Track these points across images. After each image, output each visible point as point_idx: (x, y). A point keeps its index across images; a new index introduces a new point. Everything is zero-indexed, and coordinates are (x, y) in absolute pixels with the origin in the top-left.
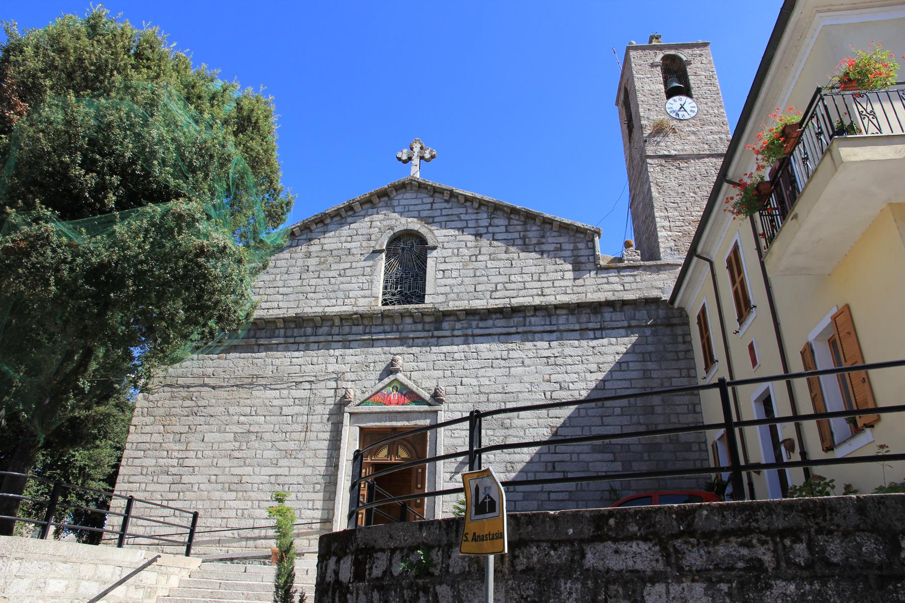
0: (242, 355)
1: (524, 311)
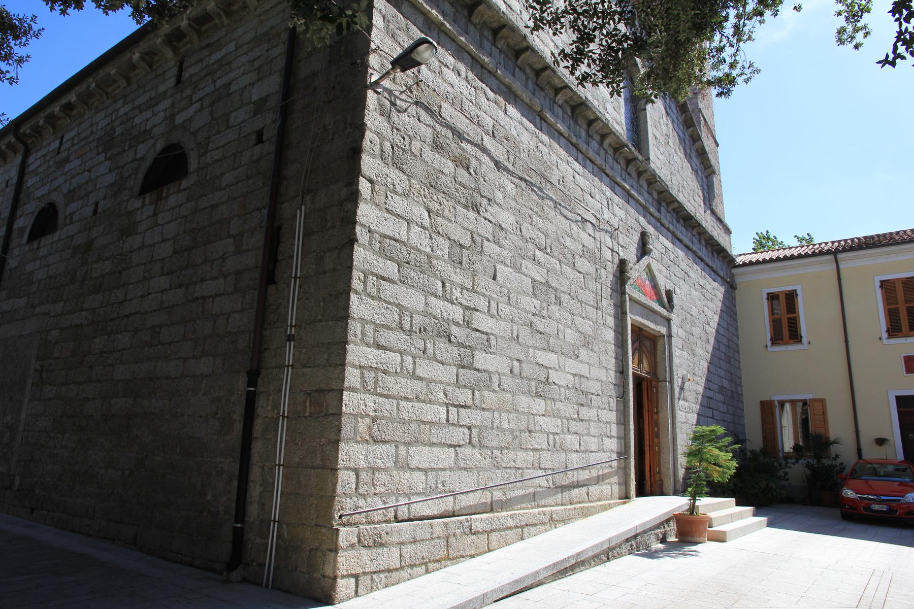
0: (525, 120)
1: (694, 227)
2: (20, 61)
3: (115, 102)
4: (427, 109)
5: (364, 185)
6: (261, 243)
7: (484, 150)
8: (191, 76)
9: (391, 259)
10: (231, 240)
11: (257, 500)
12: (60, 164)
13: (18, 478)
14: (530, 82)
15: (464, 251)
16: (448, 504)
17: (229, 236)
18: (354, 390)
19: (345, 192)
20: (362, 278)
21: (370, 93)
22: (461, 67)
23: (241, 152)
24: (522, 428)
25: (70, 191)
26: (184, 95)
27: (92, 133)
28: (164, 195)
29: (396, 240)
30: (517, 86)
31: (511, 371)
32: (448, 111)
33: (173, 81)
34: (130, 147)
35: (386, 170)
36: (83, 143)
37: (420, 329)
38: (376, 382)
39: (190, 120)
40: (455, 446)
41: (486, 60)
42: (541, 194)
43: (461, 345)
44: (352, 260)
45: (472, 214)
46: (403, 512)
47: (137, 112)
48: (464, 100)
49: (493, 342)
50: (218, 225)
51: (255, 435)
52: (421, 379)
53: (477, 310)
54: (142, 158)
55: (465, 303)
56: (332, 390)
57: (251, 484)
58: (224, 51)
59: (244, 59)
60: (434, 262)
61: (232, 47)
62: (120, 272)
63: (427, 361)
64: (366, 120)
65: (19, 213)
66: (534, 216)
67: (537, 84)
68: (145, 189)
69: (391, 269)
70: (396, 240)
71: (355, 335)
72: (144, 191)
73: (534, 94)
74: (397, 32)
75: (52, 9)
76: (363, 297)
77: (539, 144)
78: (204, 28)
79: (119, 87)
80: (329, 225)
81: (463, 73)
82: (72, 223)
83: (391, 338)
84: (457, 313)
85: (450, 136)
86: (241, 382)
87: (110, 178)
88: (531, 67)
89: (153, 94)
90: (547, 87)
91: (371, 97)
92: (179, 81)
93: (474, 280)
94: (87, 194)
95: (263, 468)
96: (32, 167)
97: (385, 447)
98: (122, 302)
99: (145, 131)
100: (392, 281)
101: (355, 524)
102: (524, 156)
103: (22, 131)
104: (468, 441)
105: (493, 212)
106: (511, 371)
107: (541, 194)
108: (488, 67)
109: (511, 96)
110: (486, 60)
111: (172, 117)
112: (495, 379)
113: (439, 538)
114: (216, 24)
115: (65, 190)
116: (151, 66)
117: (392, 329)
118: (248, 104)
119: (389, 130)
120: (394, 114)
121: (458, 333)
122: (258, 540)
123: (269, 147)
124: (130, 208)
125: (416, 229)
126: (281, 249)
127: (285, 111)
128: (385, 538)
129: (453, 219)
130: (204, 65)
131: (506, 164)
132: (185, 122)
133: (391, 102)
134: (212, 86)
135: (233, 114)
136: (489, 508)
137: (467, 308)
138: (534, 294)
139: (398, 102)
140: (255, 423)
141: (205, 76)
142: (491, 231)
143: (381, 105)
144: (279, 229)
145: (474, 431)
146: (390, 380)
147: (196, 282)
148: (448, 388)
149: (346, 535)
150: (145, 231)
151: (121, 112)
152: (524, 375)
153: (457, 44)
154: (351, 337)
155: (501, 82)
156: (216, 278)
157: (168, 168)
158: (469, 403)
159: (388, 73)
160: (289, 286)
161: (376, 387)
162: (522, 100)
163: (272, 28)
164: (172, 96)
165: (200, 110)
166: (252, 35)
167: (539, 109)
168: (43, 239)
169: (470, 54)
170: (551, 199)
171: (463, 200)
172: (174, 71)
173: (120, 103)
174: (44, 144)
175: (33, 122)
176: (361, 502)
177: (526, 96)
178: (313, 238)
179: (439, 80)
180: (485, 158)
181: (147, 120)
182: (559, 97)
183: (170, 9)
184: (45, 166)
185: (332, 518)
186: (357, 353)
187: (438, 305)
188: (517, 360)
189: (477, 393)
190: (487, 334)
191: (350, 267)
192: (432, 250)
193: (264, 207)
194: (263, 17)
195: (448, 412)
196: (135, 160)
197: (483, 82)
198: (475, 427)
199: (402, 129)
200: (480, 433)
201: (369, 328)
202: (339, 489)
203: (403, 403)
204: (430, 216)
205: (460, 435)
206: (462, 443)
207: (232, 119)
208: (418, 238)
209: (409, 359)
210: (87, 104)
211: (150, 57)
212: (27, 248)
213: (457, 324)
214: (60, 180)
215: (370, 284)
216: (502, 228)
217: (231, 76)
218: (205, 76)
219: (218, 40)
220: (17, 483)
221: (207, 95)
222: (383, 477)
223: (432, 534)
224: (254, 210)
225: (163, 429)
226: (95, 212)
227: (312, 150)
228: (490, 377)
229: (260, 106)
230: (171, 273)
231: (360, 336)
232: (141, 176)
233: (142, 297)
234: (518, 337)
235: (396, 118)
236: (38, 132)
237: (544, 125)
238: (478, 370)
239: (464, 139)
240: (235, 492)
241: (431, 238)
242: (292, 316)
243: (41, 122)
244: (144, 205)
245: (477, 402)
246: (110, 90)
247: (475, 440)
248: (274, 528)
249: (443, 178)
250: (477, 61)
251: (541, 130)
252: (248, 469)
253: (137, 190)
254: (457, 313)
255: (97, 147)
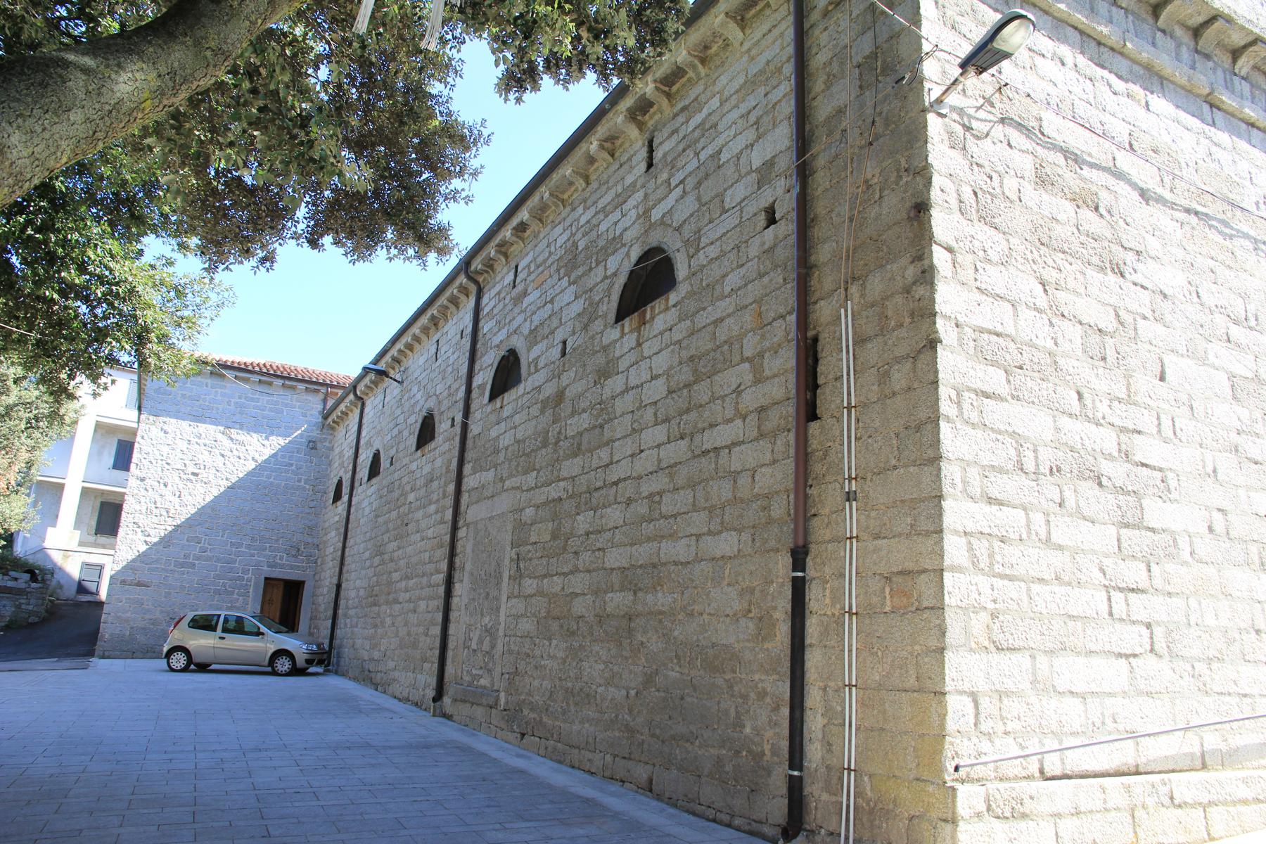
2: (475, 174)
3: (573, 210)
4: (1020, 127)
5: (939, 257)
6: (792, 363)
7: (1119, 175)
8: (665, 155)
9: (994, 364)
10: (747, 365)
11: (820, 736)
12: (518, 300)
13: (502, 695)
14: (1184, 49)
15: (1108, 339)
16: (1125, 755)
17: (743, 360)
18: (957, 569)
19: (911, 272)
20: (954, 397)
21: (931, 118)
22: (1065, 51)
23: (746, 242)
24: (1243, 625)
25: (531, 332)
26: (659, 181)
27: (550, 254)
28: (648, 316)
29: (998, 335)
30: (1164, 61)
31: (1211, 529)
32: (1054, 125)
33: (643, 166)
34: (598, 264)
35: (970, 230)
36: (541, 269)
37: (1051, 470)
38: (991, 556)
39: (670, 211)
40: (1127, 656)
41: (1105, 30)
42: (1228, 231)
43: (1122, 490)
44: (936, 372)
45: (1112, 279)
46: (1053, 767)
47: (601, 216)
48: (1077, 102)
49: (1173, 483)
50: (726, 347)
51: (808, 641)
52: (1060, 548)
53: (1139, 432)
54: (615, 274)
55: (1118, 422)
56: (924, 571)
57: (808, 713)
58: (705, 111)
59: (735, 115)
60: (1061, 362)
61: (715, 103)
62: (602, 427)
63: (1068, 520)
64: (930, 160)
65: (477, 367)
66: (1220, 269)
67: (1197, 51)
68: (622, 314)
69: (994, 379)
70: (998, 335)
71: (953, 485)
72: (621, 316)
73: (1193, 67)
74: (959, 19)
75: (506, 100)
76: (959, 426)
77: (1214, 149)
78: (674, 88)
79: (576, 190)
80: (893, 323)
81: (1069, 61)
82: (537, 371)
83: (1004, 486)
84: (1107, 440)
85: (1062, 161)
86: (782, 565)
87: (578, 307)
88: (1184, 26)
89: (619, 189)
90: (1217, 52)
91: (934, 124)
92: (650, 165)
93: (1129, 384)
94: (552, 332)
95: (824, 690)
96: (486, 310)
97: (1016, 657)
98: (607, 465)
99: (614, 239)
100: (1000, 398)
101: (978, 780)
102: (1187, 173)
103: (473, 268)
104: (1148, 648)
105: (1147, 272)
106: (1211, 529)
107: (1228, 231)
108: (1109, 43)
109: (1153, 78)
110: (1105, 30)
111: (647, 213)
112: (1183, 543)
113: (1117, 809)
114: (690, 80)
115: (526, 332)
116: (612, 156)
117: (1007, 472)
118: (748, 173)
119: (967, 169)
120: (971, 141)
121: (1115, 471)
122: (825, 797)
123: (787, 227)
124: (605, 341)
125: (1026, 314)
126: (821, 368)
127: (804, 172)
128: (1029, 806)
129: (1082, 290)
130: (681, 136)
131: (1160, 190)
132: (663, 216)
133: (964, 126)
134: (695, 160)
135: (729, 193)
136: (1198, 763)
137: (1123, 430)
138: (1235, 398)
139: (975, 124)
140: (808, 623)
141: (684, 150)
142: (1148, 303)
143: (951, 134)
144: (816, 340)
145: (1159, 632)
146: (1012, 553)
147: (704, 430)
148: (1106, 561)
149: (968, 799)
150: (628, 369)
151: (582, 221)
152: (1233, 534)
153: (1054, 18)
154: (946, 489)
155: (1134, 61)
156: (731, 420)
157: (649, 281)
158: (1143, 584)
159: (955, 82)
160: (839, 420)
161: (992, 564)
162: (1173, 83)
163: (768, 63)
164: (643, 186)
165: (682, 197)
166: (741, 80)
167: (1207, 91)
168: (506, 395)
169: (1076, 28)
170: (1246, 236)
171: (1095, 260)
172: (643, 153)
173: (580, 209)
174: (498, 279)
175: (483, 254)
176: (985, 746)
177: (1179, 73)
178: (870, 346)
179: (1032, 77)
180: (1122, 188)
181: (616, 223)
182: (1240, 63)
183: (643, 63)
184: (501, 306)
185: (941, 770)
186: (957, 512)
187: (1075, 430)
188: (1219, 510)
189: (1154, 567)
190: (1160, 470)
191: (935, 383)
192: (1056, 344)
193: (790, 313)
194: (753, 52)
195: (1109, 599)
196: (606, 277)
197: (1103, 67)
198: (1158, 624)
199: (986, 164)
200: (1169, 632)
201: (973, 473)
202: (951, 725)
203: (1036, 588)
204: (1045, 291)
205: (1133, 638)
206: (1138, 650)
207: (727, 199)
208: (1030, 326)
209: (1038, 518)
210: (540, 220)
211: (611, 144)
212: (489, 408)
213: (1109, 457)
214: (520, 319)
215: (966, 406)
216: (1165, 296)
217: (720, 141)
218: (684, 150)
219: (696, 99)
220: (502, 701)
221: (690, 174)
222: (1013, 707)
223: (1105, 801)
224: (774, 320)
225: (676, 633)
226: (564, 353)
227: (851, 220)
228: (1175, 541)
229: (765, 174)
230: (667, 420)
231: (960, 486)
232: (615, 297)
233: (632, 456)
234: (1214, 471)
235: (975, 149)
236: (490, 265)
237: (1218, 115)
238: (1153, 530)
239: (1085, 162)
240: (786, 724)
241: (1051, 324)
242: (850, 462)
243: (493, 253)
244: (623, 334)
245: (1158, 582)
246: (565, 196)
247: (1160, 646)
248: (849, 780)
249: (1059, 228)
250: (1089, 36)
251: (1214, 124)
252: (803, 689)
253: (612, 316)
254: (1107, 440)
255: (558, 270)
